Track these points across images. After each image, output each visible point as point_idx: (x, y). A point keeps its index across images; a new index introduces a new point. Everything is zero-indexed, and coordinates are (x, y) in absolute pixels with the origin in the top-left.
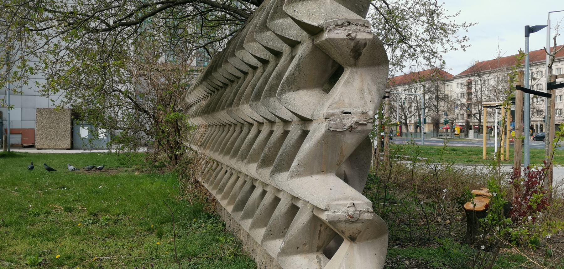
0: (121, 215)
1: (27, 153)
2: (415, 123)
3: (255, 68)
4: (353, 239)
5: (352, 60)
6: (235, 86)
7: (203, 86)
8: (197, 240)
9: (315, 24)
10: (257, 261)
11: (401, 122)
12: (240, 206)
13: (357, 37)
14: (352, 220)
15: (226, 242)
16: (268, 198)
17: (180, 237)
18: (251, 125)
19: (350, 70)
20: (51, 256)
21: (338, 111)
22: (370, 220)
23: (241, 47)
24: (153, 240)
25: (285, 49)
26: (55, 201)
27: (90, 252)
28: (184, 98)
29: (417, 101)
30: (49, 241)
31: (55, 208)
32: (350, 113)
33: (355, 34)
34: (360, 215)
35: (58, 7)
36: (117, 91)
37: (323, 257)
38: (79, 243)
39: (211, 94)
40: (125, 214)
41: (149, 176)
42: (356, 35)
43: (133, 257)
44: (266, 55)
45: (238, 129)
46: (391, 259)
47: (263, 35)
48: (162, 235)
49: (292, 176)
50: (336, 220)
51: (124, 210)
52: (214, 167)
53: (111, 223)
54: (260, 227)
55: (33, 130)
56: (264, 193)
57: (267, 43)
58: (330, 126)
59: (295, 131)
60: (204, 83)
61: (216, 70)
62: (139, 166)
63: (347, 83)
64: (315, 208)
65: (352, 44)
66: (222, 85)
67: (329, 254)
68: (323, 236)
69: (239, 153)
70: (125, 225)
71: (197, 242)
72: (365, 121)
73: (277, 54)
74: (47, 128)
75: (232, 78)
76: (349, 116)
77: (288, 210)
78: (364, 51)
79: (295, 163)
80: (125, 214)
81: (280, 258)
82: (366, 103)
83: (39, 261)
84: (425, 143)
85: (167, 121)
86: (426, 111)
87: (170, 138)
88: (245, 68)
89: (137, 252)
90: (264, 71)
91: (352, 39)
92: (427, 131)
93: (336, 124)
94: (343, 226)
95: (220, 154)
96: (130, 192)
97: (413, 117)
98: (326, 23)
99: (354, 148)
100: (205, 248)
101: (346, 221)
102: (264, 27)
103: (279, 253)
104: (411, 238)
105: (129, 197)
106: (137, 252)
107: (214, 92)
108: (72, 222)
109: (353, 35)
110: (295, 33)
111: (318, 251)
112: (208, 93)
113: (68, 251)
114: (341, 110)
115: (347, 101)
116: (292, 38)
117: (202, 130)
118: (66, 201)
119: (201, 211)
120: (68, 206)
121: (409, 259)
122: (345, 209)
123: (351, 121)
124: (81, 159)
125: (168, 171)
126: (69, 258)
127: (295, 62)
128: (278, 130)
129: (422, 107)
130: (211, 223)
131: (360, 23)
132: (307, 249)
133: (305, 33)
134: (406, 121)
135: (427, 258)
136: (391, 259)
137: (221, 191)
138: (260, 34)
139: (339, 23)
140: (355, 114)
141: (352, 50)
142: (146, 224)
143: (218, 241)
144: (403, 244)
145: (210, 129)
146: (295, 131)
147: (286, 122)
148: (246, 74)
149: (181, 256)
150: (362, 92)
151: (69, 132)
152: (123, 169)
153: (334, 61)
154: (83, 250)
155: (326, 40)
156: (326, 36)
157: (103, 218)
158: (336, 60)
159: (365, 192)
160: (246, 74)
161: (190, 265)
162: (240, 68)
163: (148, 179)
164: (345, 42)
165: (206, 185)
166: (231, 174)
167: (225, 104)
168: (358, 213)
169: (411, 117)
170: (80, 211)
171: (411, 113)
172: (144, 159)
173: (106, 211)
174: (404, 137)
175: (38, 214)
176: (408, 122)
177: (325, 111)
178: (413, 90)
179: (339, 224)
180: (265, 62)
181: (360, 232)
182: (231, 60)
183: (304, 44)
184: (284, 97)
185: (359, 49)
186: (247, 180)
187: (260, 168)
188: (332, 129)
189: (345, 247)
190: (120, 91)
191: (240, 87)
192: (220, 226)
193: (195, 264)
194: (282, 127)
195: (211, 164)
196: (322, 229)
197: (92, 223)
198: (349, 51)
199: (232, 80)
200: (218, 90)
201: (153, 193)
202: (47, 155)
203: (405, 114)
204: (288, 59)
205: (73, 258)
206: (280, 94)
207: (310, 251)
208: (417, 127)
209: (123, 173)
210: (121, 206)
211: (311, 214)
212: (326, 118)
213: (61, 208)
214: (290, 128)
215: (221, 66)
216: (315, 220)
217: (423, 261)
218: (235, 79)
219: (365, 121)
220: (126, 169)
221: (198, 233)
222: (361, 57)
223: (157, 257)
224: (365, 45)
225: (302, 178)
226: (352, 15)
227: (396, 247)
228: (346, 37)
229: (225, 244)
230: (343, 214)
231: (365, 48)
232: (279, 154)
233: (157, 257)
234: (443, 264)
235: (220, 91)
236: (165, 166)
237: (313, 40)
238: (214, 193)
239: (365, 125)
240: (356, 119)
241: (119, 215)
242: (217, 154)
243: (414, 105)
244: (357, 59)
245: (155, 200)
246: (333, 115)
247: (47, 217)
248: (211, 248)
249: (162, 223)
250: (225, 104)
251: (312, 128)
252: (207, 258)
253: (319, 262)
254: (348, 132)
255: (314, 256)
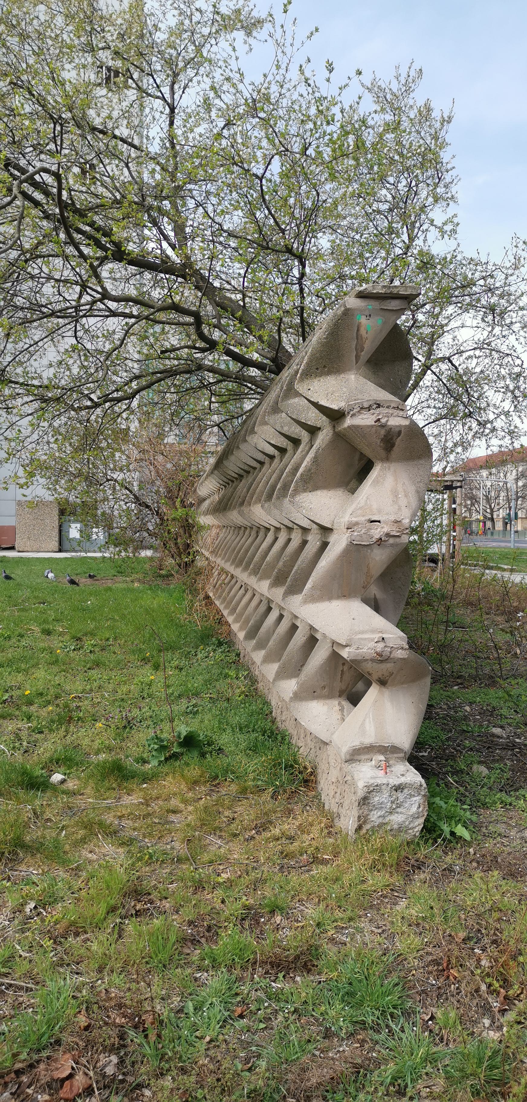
0: (111, 640)
1: (4, 557)
2: (504, 518)
3: (272, 457)
4: (383, 683)
5: (383, 453)
6: (250, 479)
7: (212, 480)
8: (201, 674)
9: (335, 406)
10: (273, 703)
11: (485, 517)
12: (251, 634)
13: (389, 423)
14: (381, 658)
15: (237, 678)
16: (284, 626)
17: (181, 669)
18: (268, 530)
19: (380, 465)
20: (18, 692)
21: (363, 519)
22: (404, 659)
23: (253, 432)
24: (148, 674)
25: (305, 436)
26: (31, 620)
27: (68, 688)
28: (195, 490)
29: (507, 489)
30: (19, 672)
31: (30, 630)
32: (379, 522)
33: (386, 419)
34: (391, 653)
35: (33, 378)
36: (111, 480)
37: (346, 704)
38: (55, 676)
39: (225, 486)
40: (115, 639)
41: (150, 589)
42: (387, 421)
43: (119, 696)
44: (282, 442)
45: (254, 533)
46: (447, 704)
47: (277, 416)
48: (159, 666)
49: (305, 602)
50: (360, 658)
51: (115, 633)
52: (226, 581)
53: (97, 649)
54: (274, 661)
55: (14, 528)
56: (281, 617)
57: (282, 427)
58: (353, 538)
59: (314, 541)
60: (216, 472)
61: (227, 458)
62: (140, 576)
63: (376, 482)
64: (333, 643)
65: (383, 432)
66: (236, 476)
67: (355, 699)
68: (347, 677)
69: (251, 566)
70: (115, 653)
71: (200, 678)
72: (398, 532)
73: (296, 442)
74: (30, 526)
75: (246, 468)
76: (378, 526)
77: (305, 643)
78: (398, 442)
79: (309, 585)
80: (115, 639)
81: (292, 704)
82: (400, 509)
83: (4, 698)
84: (516, 545)
85: (174, 519)
86: (519, 502)
87: (179, 541)
88: (261, 457)
89: (125, 689)
90: (281, 461)
91: (383, 426)
92: (519, 528)
93: (361, 536)
94: (369, 667)
95: (231, 565)
96: (125, 609)
97: (501, 510)
98: (349, 405)
99: (385, 566)
100: (210, 684)
101: (372, 660)
102: (276, 409)
103: (291, 698)
104: (477, 675)
105: (123, 617)
106: (125, 689)
107: (228, 484)
108: (50, 648)
109: (383, 421)
110: (314, 417)
111: (340, 696)
112: (221, 485)
113: (40, 686)
114: (367, 518)
115: (375, 506)
116: (309, 423)
117: (214, 531)
118: (44, 621)
119: (209, 636)
120: (47, 627)
121: (471, 704)
122: (372, 644)
123: (380, 532)
124: (69, 565)
125: (174, 584)
126: (41, 694)
127: (311, 455)
128: (296, 538)
129: (514, 497)
130: (221, 652)
131: (393, 405)
132: (327, 694)
133: (324, 418)
134: (492, 515)
135: (494, 703)
136: (447, 704)
137: (233, 611)
138: (273, 417)
139: (366, 405)
140: (386, 523)
141: (382, 440)
142: (141, 653)
143: (226, 676)
144: (466, 684)
145: (224, 530)
146: (314, 541)
147: (305, 530)
148: (262, 463)
149: (179, 695)
150: (395, 494)
151: (57, 530)
152: (121, 579)
153: (361, 453)
154: (59, 685)
155: (349, 427)
156: (348, 422)
157: (88, 643)
158: (364, 452)
159: (400, 625)
160: (262, 463)
161: (188, 707)
162: (254, 456)
163: (149, 592)
164: (374, 430)
165: (217, 603)
166: (246, 591)
167: (237, 502)
168: (389, 650)
169: (499, 510)
170: (61, 634)
171: (498, 504)
172: (147, 566)
173: (92, 634)
174: (489, 536)
175: (9, 637)
176: (495, 516)
177: (346, 519)
178: (502, 475)
179: (364, 664)
180: (282, 451)
181: (391, 674)
182: (243, 446)
183: (324, 431)
184: (298, 498)
185: (392, 439)
186: (263, 599)
187: (272, 587)
188: (355, 543)
189: (373, 693)
190: (116, 481)
191: (254, 480)
192: (233, 656)
193: (195, 706)
194: (300, 535)
195: (224, 577)
196: (346, 668)
197: (74, 650)
198: (379, 441)
199: (247, 471)
200: (233, 481)
201: (153, 611)
202: (29, 559)
203: (490, 506)
204: (307, 448)
205: (46, 695)
206: (293, 496)
207: (330, 696)
208: (507, 523)
209: (120, 584)
210: (111, 628)
211: (331, 649)
212: (348, 529)
213: (36, 629)
214: (310, 538)
215: (232, 453)
216: (335, 657)
217: (489, 708)
218: (252, 470)
219: (398, 532)
220: (124, 579)
221: (204, 665)
222: (394, 449)
223: (150, 696)
224: (400, 432)
225: (317, 604)
226: (383, 395)
227: (456, 688)
228: (373, 423)
229: (235, 680)
230: (369, 651)
231: (400, 438)
232: (293, 572)
233: (150, 696)
234: (515, 711)
235: (235, 483)
236: (172, 575)
237: (334, 427)
238: (225, 613)
239: (398, 536)
240: (386, 529)
241: (108, 640)
242: (229, 564)
243: (503, 494)
244: (390, 451)
245: (154, 621)
246: (357, 524)
247: (19, 641)
248: (218, 686)
249: (160, 651)
250: (237, 502)
251: (332, 539)
252: (211, 698)
253: (342, 710)
254: (376, 545)
255: (335, 702)
